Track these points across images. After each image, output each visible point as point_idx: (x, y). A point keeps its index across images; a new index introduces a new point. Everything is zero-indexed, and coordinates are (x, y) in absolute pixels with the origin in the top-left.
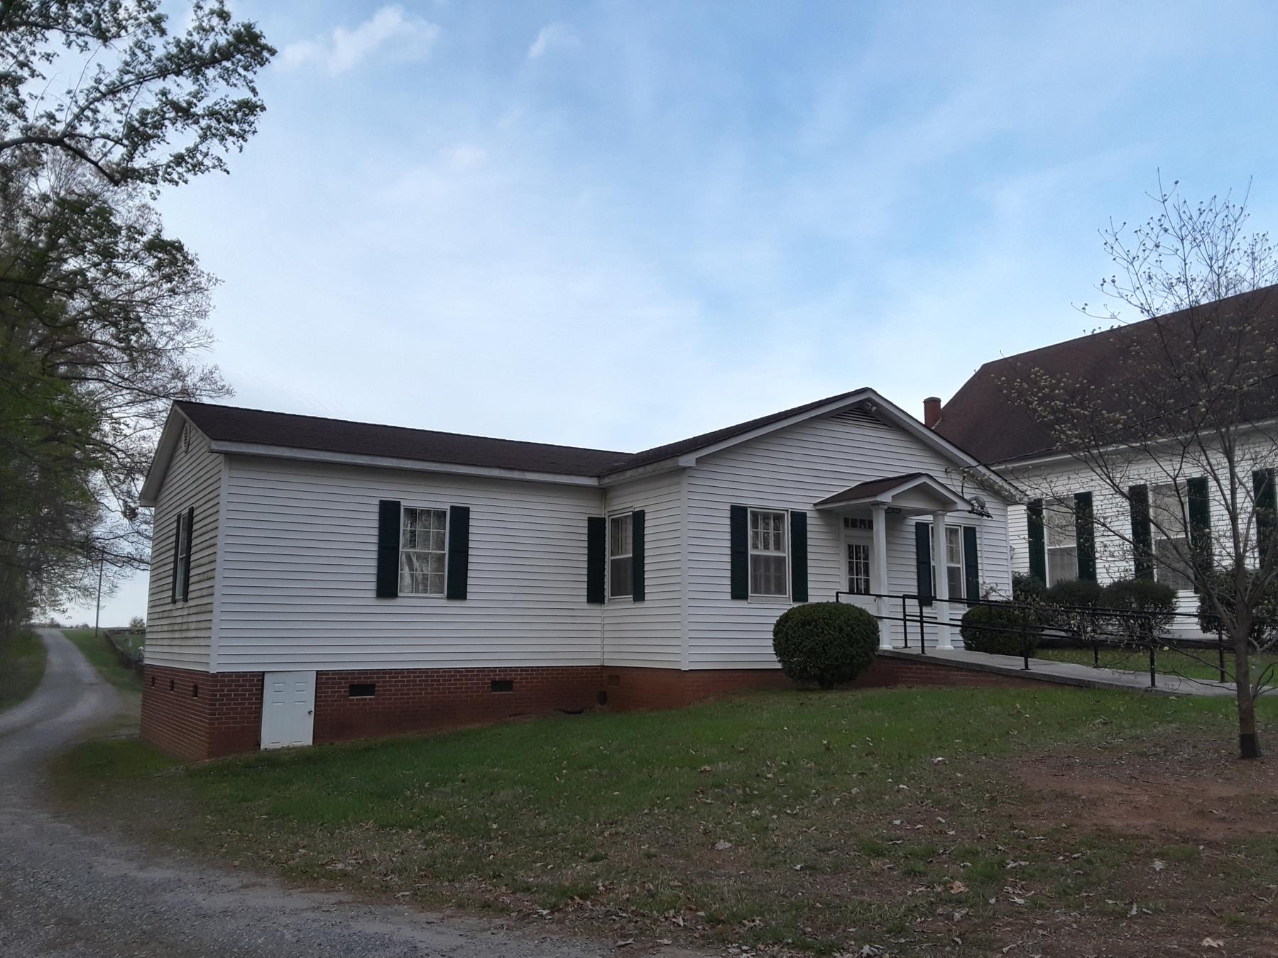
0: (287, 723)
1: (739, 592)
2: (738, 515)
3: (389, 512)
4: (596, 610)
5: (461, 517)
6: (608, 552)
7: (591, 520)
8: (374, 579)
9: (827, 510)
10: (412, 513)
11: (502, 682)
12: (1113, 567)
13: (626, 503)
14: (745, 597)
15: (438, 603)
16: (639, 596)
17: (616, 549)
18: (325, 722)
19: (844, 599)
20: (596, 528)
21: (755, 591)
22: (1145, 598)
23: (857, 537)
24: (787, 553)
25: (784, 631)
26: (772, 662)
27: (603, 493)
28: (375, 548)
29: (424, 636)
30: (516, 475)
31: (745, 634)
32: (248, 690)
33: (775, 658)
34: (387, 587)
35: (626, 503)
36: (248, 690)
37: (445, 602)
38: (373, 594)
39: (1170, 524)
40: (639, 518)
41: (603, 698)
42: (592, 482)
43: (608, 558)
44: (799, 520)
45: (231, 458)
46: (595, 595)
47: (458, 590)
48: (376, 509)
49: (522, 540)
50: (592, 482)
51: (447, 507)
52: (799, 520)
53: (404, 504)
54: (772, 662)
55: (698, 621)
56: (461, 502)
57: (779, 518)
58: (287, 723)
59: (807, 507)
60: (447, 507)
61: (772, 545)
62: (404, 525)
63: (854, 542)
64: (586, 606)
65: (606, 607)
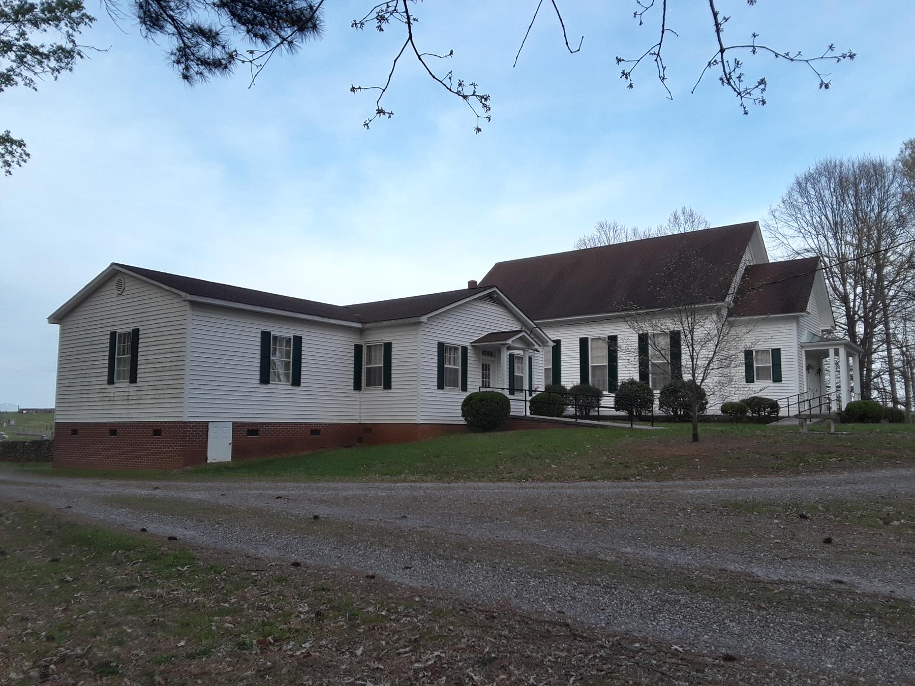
0: (219, 449)
1: (441, 386)
2: (441, 347)
3: (265, 336)
4: (357, 394)
5: (298, 340)
6: (364, 363)
7: (356, 346)
8: (258, 373)
9: (476, 345)
10: (275, 338)
11: (315, 430)
12: (570, 378)
13: (379, 337)
14: (442, 388)
15: (287, 387)
16: (388, 385)
17: (369, 361)
18: (238, 449)
19: (482, 390)
20: (358, 349)
21: (758, 379)
22: (586, 395)
23: (488, 360)
24: (459, 367)
25: (469, 406)
26: (462, 421)
27: (361, 332)
28: (259, 356)
29: (282, 405)
30: (326, 320)
31: (447, 406)
32: (201, 430)
33: (463, 419)
34: (265, 379)
35: (379, 337)
36: (201, 430)
37: (290, 387)
38: (258, 382)
39: (598, 358)
40: (388, 347)
41: (360, 440)
42: (358, 325)
43: (364, 367)
44: (465, 349)
45: (193, 304)
46: (357, 386)
47: (296, 382)
48: (260, 335)
49: (326, 353)
50: (358, 325)
51: (291, 336)
52: (465, 349)
53: (272, 333)
54: (462, 421)
55: (420, 398)
56: (298, 334)
57: (456, 349)
58: (219, 449)
59: (467, 344)
60: (291, 336)
61: (452, 363)
62: (516, 361)
63: (485, 362)
64: (353, 392)
65: (362, 392)
